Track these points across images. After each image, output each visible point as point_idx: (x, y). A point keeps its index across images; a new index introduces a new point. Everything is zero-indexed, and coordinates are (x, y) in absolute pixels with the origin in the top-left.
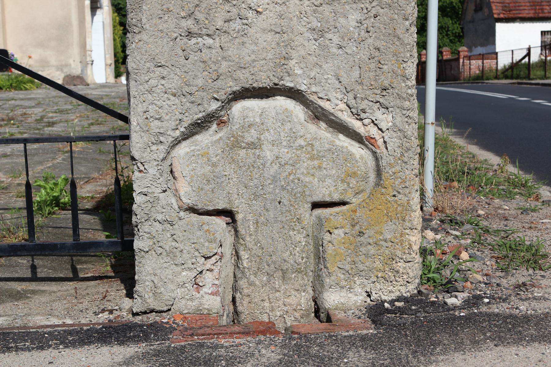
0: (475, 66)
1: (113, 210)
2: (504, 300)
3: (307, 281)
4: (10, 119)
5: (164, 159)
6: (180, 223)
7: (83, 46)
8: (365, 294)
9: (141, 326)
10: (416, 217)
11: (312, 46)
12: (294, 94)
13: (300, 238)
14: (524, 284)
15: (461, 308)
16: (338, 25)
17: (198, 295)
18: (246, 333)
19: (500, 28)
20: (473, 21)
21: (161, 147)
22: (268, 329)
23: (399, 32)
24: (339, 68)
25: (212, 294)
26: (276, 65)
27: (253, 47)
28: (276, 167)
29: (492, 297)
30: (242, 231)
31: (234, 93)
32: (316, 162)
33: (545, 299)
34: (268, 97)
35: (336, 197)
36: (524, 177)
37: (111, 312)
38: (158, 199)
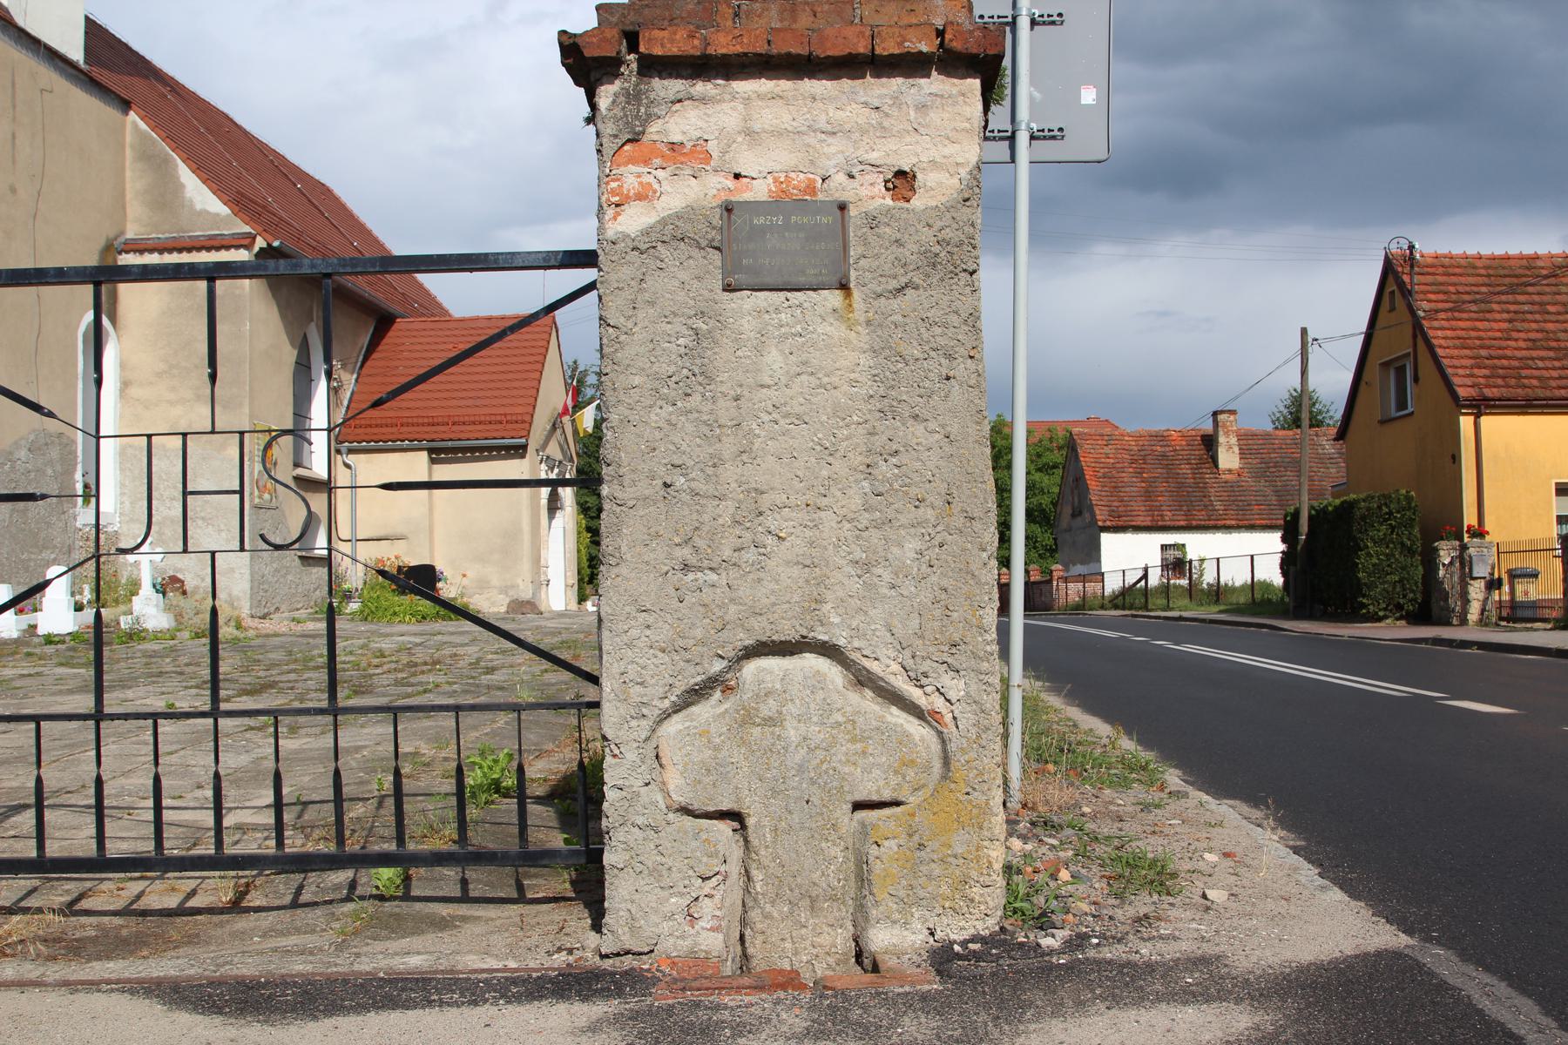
0: (1074, 591)
1: (575, 799)
2: (1119, 941)
3: (846, 912)
4: (435, 663)
5: (647, 739)
6: (668, 829)
7: (537, 562)
8: (927, 932)
9: (613, 974)
10: (999, 819)
11: (855, 585)
12: (829, 650)
13: (836, 851)
14: (1146, 916)
15: (1060, 952)
16: (889, 556)
17: (692, 932)
18: (760, 988)
19: (1107, 539)
20: (1069, 530)
21: (644, 723)
22: (788, 981)
23: (973, 567)
24: (891, 614)
25: (712, 929)
26: (805, 610)
27: (773, 586)
28: (803, 752)
29: (1102, 936)
30: (754, 841)
31: (746, 648)
32: (859, 746)
33: (1175, 938)
34: (792, 654)
35: (887, 795)
36: (1146, 755)
37: (570, 951)
38: (638, 795)
